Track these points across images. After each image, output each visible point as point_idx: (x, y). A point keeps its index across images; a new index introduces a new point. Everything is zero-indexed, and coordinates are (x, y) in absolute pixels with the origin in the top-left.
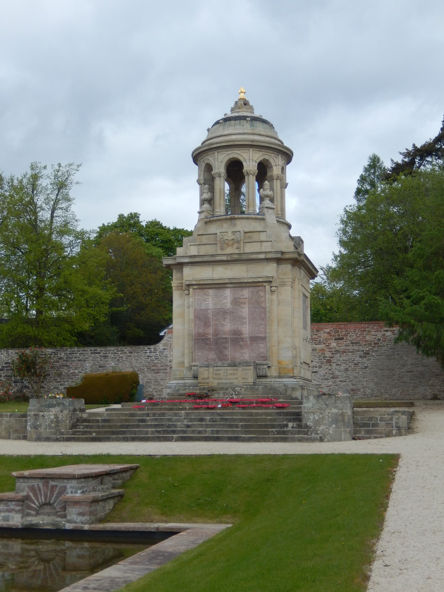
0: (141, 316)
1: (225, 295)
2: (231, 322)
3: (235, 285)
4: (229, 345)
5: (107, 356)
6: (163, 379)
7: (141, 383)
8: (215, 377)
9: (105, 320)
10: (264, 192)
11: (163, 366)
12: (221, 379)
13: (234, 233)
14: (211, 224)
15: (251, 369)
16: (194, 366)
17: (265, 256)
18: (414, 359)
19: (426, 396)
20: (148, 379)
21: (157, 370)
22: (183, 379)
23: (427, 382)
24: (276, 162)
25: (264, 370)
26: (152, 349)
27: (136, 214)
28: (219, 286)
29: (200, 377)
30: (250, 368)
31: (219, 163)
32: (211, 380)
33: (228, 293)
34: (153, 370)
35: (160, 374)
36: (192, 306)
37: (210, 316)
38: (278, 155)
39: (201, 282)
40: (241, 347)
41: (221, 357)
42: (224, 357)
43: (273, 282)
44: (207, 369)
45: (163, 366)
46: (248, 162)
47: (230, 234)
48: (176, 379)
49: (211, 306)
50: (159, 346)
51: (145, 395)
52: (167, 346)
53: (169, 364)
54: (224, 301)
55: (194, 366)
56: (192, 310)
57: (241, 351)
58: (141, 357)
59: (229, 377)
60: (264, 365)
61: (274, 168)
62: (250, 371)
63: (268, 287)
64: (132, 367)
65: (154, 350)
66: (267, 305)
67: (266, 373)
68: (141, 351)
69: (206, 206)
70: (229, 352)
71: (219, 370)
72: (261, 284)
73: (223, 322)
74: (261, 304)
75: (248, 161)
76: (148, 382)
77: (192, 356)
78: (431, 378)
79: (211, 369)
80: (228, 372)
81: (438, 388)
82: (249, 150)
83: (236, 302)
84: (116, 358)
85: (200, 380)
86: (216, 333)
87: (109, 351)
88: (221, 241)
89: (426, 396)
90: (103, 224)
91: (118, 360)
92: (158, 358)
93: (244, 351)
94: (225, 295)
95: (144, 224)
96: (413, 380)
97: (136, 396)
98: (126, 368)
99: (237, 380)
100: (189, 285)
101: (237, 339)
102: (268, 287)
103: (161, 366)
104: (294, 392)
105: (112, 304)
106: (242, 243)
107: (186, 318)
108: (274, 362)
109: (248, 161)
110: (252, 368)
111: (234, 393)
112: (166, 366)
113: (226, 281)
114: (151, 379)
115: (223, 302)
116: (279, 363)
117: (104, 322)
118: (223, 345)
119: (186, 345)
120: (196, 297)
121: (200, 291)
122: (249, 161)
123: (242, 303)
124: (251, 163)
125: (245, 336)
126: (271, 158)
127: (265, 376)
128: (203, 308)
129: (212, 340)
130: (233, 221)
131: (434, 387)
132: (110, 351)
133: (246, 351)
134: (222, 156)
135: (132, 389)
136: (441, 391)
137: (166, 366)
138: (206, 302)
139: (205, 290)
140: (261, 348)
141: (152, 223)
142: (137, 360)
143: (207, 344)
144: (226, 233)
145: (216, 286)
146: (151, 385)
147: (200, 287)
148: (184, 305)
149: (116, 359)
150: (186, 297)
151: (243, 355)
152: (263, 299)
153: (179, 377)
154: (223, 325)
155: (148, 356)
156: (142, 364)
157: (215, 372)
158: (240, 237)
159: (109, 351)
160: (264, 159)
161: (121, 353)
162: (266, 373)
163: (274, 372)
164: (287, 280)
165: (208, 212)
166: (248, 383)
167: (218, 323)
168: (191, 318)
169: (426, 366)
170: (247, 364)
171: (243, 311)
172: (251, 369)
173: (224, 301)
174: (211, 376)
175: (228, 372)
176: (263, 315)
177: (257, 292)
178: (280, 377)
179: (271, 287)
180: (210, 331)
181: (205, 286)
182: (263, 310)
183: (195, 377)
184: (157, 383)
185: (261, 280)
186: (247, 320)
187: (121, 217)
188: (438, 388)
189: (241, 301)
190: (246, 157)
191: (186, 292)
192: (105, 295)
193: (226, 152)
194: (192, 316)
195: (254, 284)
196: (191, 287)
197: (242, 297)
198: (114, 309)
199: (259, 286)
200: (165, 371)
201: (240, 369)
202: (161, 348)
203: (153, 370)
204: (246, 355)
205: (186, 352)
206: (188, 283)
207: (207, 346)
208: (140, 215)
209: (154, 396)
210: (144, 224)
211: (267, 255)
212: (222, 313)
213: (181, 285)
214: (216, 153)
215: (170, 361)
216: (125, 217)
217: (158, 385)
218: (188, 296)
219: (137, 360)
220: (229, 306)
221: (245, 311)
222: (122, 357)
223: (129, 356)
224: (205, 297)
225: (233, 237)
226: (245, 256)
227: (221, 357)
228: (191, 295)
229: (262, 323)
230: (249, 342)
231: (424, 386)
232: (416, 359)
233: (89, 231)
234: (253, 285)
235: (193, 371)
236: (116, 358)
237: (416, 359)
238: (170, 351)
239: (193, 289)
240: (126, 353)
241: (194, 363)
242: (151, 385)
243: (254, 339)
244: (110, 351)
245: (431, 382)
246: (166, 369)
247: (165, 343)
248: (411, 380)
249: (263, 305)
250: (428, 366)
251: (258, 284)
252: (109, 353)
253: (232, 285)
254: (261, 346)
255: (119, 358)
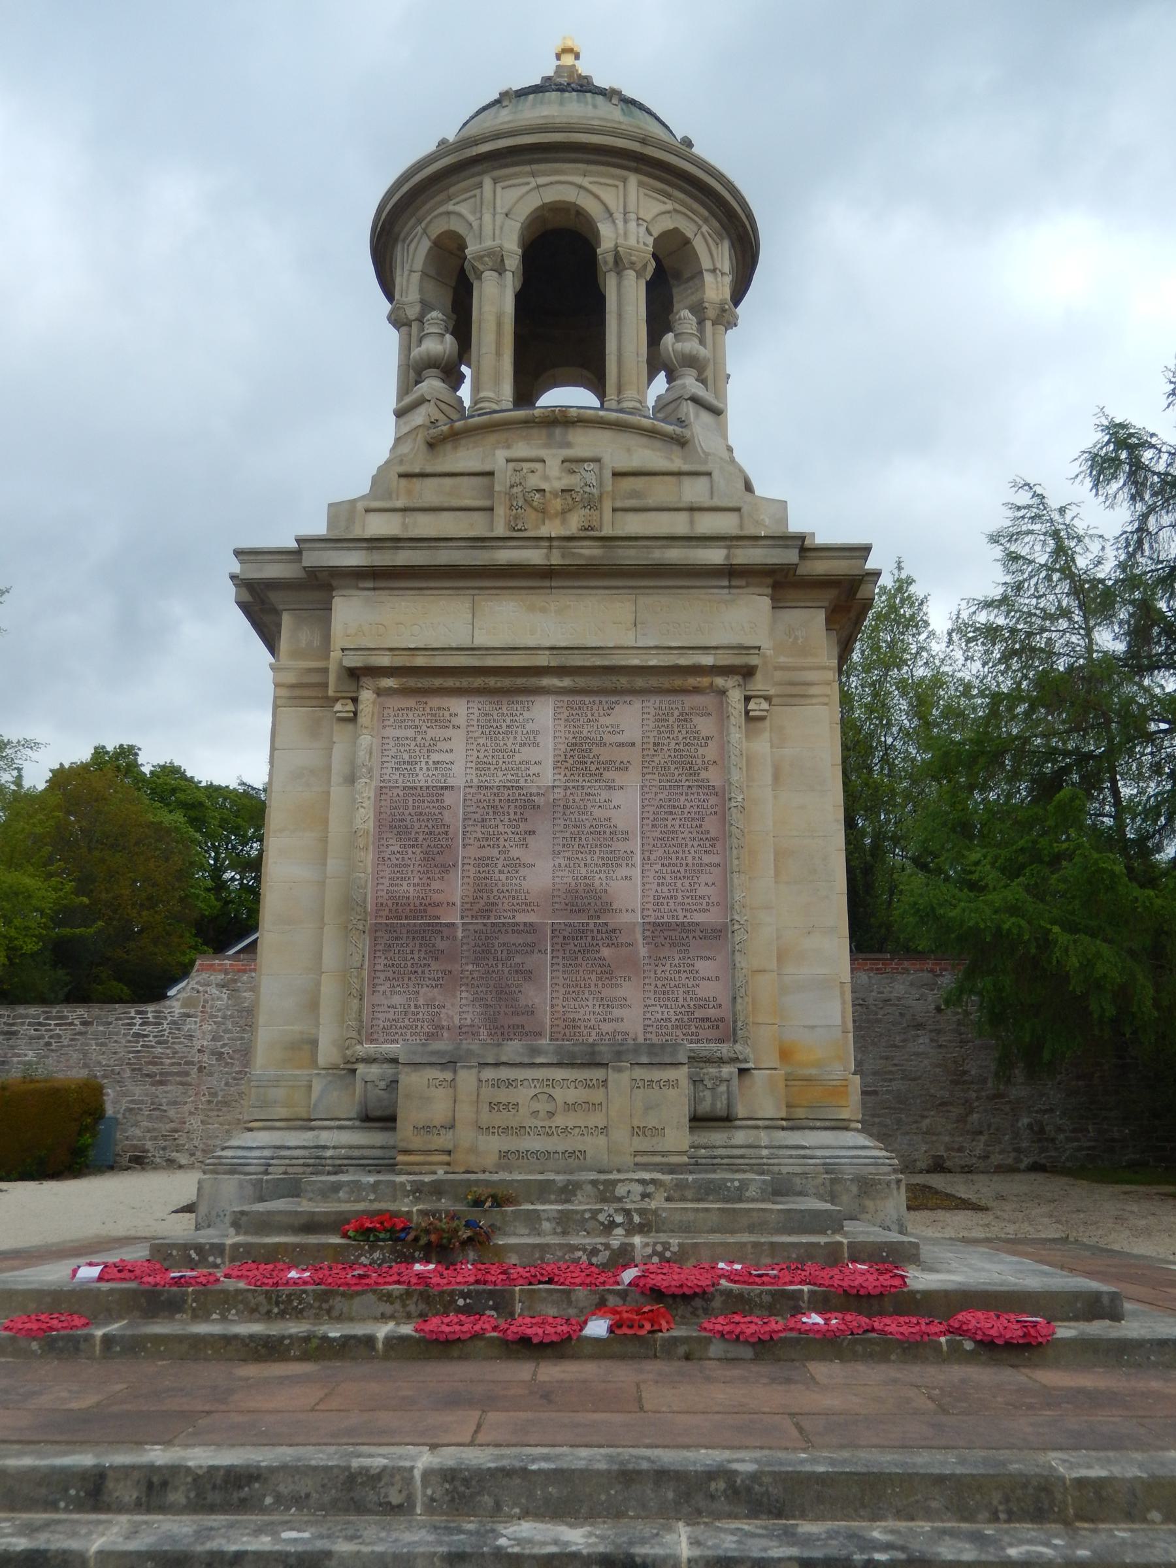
0: (127, 952)
1: (530, 726)
2: (555, 854)
3: (581, 682)
4: (545, 962)
5: (15, 1033)
6: (175, 1103)
7: (110, 1111)
8: (486, 1117)
9: (35, 948)
10: (679, 346)
11: (180, 1064)
12: (520, 1130)
13: (574, 466)
14: (455, 448)
15: (675, 1084)
16: (369, 1060)
17: (728, 557)
18: (881, 1058)
19: (915, 1161)
20: (132, 1101)
21: (161, 1074)
22: (306, 1123)
23: (916, 1122)
24: (714, 257)
25: (723, 1088)
26: (150, 1015)
27: (131, 747)
28: (501, 680)
29: (409, 1116)
30: (670, 1074)
31: (500, 218)
32: (465, 1135)
33: (543, 714)
34: (147, 1075)
35: (169, 1088)
36: (370, 770)
37: (456, 818)
38: (722, 239)
39: (420, 661)
40: (607, 973)
41: (506, 1018)
42: (517, 1020)
43: (759, 676)
44: (448, 1075)
45: (180, 1064)
46: (620, 223)
47: (553, 467)
48: (269, 1125)
49: (460, 773)
50: (171, 1007)
51: (118, 1148)
52: (195, 1006)
53: (196, 1060)
54: (527, 753)
55: (369, 1060)
56: (366, 790)
57: (606, 992)
58: (115, 1038)
59: (560, 1121)
60: (721, 1061)
61: (708, 278)
62: (671, 1093)
63: (735, 697)
64: (86, 1066)
65: (155, 1017)
66: (735, 776)
67: (729, 1106)
68: (117, 1019)
69: (432, 385)
70: (544, 997)
71: (510, 1083)
72: (705, 681)
73: (515, 852)
74: (704, 774)
75: (619, 216)
76: (131, 1110)
77: (360, 1011)
78: (926, 1113)
79: (467, 1078)
80: (557, 1093)
81: (947, 1139)
82: (625, 180)
83: (581, 759)
84: (41, 1037)
85: (405, 1132)
86: (482, 904)
87: (21, 1016)
88: (512, 497)
89: (915, 1161)
90: (61, 764)
91: (48, 1044)
92: (166, 1042)
93: (620, 993)
94: (530, 726)
95: (146, 770)
96: (878, 1116)
97: (91, 1153)
98: (70, 1068)
99: (602, 1140)
100: (354, 675)
101: (584, 929)
102: (735, 697)
103: (173, 1064)
104: (869, 1204)
105: (64, 915)
106: (607, 505)
107: (336, 829)
108: (761, 1050)
109: (619, 216)
110: (681, 1074)
111: (619, 1219)
112: (187, 1063)
113: (542, 660)
114: (142, 1102)
115: (518, 758)
116: (785, 1054)
117: (33, 955)
118: (518, 959)
119: (331, 957)
120: (390, 732)
121: (411, 702)
122: (626, 221)
123: (609, 764)
124: (632, 225)
125: (625, 918)
126: (699, 236)
127: (726, 1120)
128: (421, 780)
129: (460, 934)
130: (558, 431)
131: (934, 1138)
132: (27, 1016)
133: (628, 990)
134: (514, 194)
135: (80, 1134)
136: (952, 1149)
137: (187, 1063)
138: (435, 757)
139: (435, 702)
140: (707, 978)
141: (163, 767)
142: (102, 1044)
143: (436, 955)
144: (538, 466)
145: (492, 682)
146: (139, 1118)
147: (412, 682)
148: (328, 769)
149: (42, 1042)
150: (342, 734)
151: (616, 1012)
152: (710, 752)
153: (283, 1112)
154: (516, 865)
155: (136, 1035)
156: (117, 1057)
157: (487, 1093)
158: (601, 484)
159: (21, 1016)
160: (676, 231)
161: (56, 1025)
162: (729, 1106)
163: (762, 1098)
164: (811, 676)
165: (442, 406)
166: (664, 1154)
167: (495, 853)
168: (359, 824)
169: (914, 1079)
170: (657, 1055)
171: (615, 803)
172: (675, 1084)
173: (527, 753)
174: (465, 1112)
175: (557, 1093)
176: (711, 825)
177: (685, 718)
178: (793, 1124)
179: (748, 699)
180: (455, 890)
181: (438, 682)
182: (713, 800)
183: (381, 1118)
184: (157, 1113)
185: (707, 660)
186: (636, 845)
187: (99, 752)
188: (947, 1139)
189: (605, 754)
190: (612, 205)
191: (342, 708)
192: (39, 889)
193: (532, 179)
194: (365, 818)
195: (673, 680)
196: (366, 681)
197: (608, 738)
198: (66, 931)
199: (696, 690)
200: (184, 1079)
201: (620, 1080)
202: (177, 1011)
203: (147, 1075)
204: (631, 1011)
205: (329, 989)
206: (353, 661)
207: (434, 966)
208: (139, 749)
209: (148, 1151)
210: (146, 770)
211: (738, 552)
212: (513, 807)
213: (315, 678)
214: (487, 182)
215: (199, 1051)
216: (107, 753)
217: (160, 1119)
218: (350, 727)
219: (102, 1044)
220: (548, 775)
221: (626, 803)
222: (59, 1036)
223: (80, 1033)
224: (431, 733)
225: (567, 481)
226: (632, 552)
227: (506, 1018)
228: (363, 719)
229: (706, 859)
230: (643, 951)
231: (908, 1133)
232: (887, 1058)
233: (15, 741)
234: (666, 682)
235: (359, 1086)
236: (41, 1037)
237: (887, 1058)
238: (202, 1021)
239: (379, 692)
240: (71, 1024)
241: (367, 1048)
242: (139, 1118)
243: (670, 936)
244: (27, 1016)
245: (927, 1121)
246: (187, 1074)
247: (189, 997)
248: (873, 1116)
249: (712, 776)
250: (919, 1078)
251: (692, 681)
252: (23, 1024)
253: (566, 682)
254: (704, 967)
255: (51, 1037)
